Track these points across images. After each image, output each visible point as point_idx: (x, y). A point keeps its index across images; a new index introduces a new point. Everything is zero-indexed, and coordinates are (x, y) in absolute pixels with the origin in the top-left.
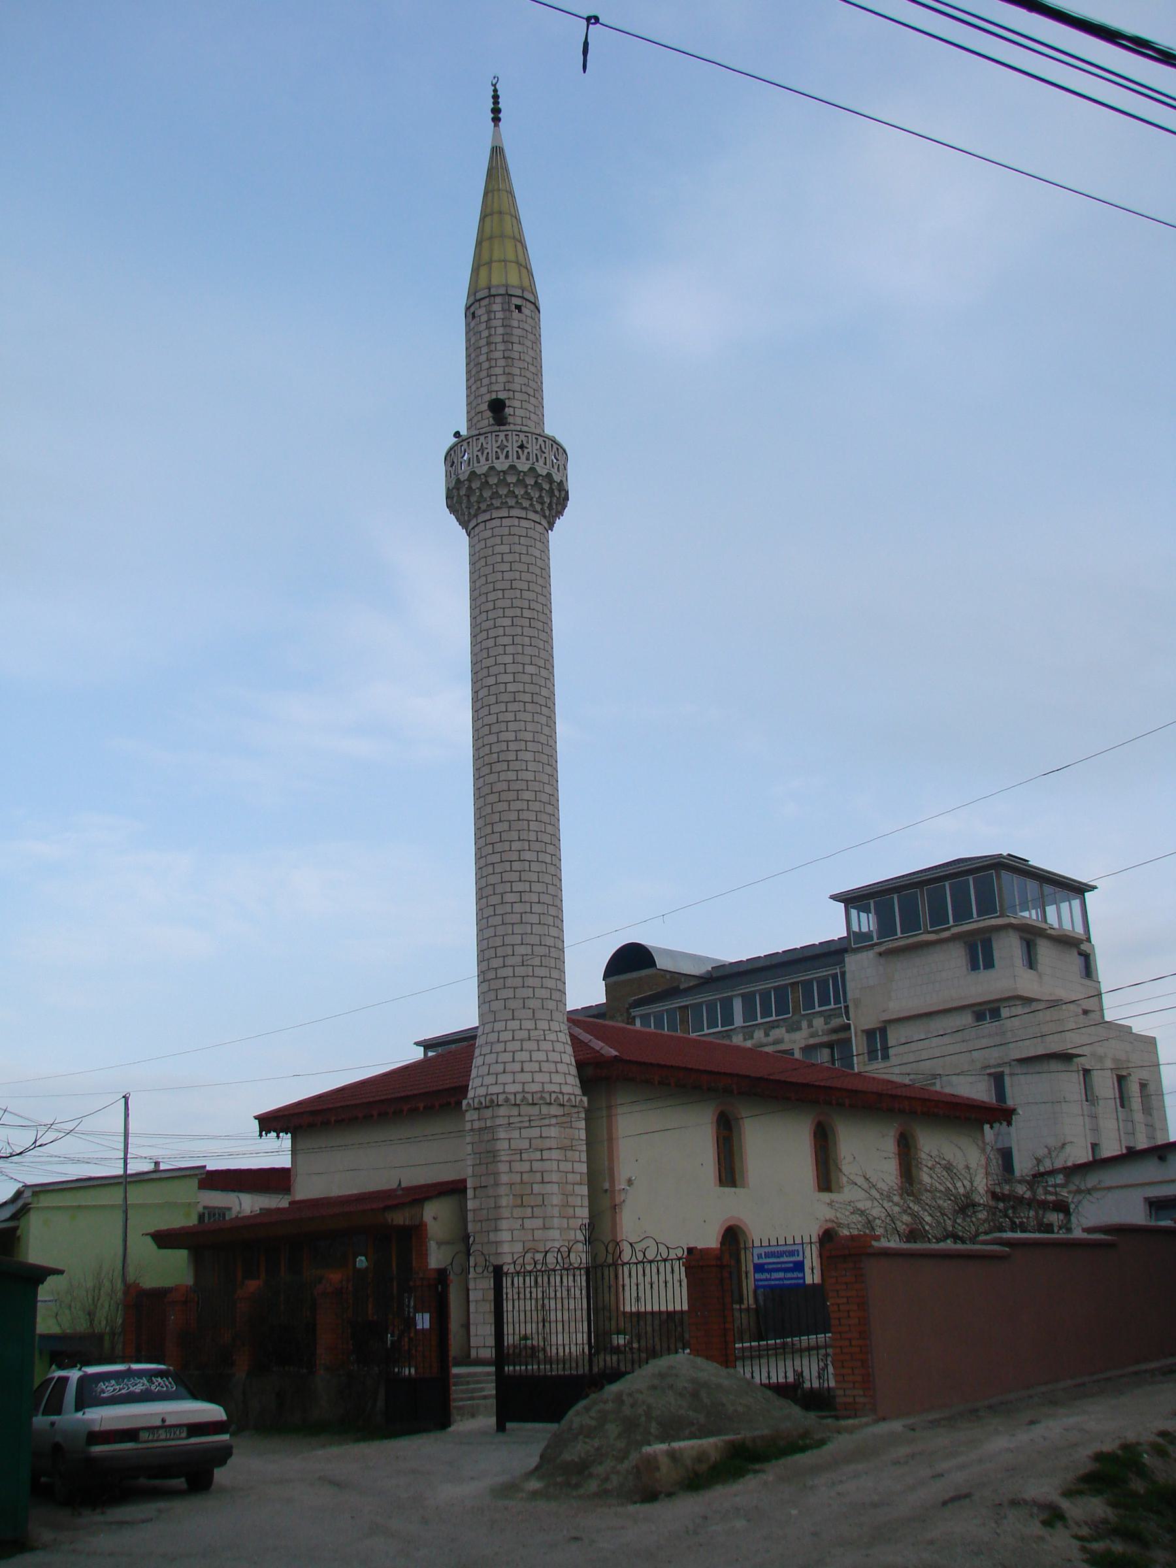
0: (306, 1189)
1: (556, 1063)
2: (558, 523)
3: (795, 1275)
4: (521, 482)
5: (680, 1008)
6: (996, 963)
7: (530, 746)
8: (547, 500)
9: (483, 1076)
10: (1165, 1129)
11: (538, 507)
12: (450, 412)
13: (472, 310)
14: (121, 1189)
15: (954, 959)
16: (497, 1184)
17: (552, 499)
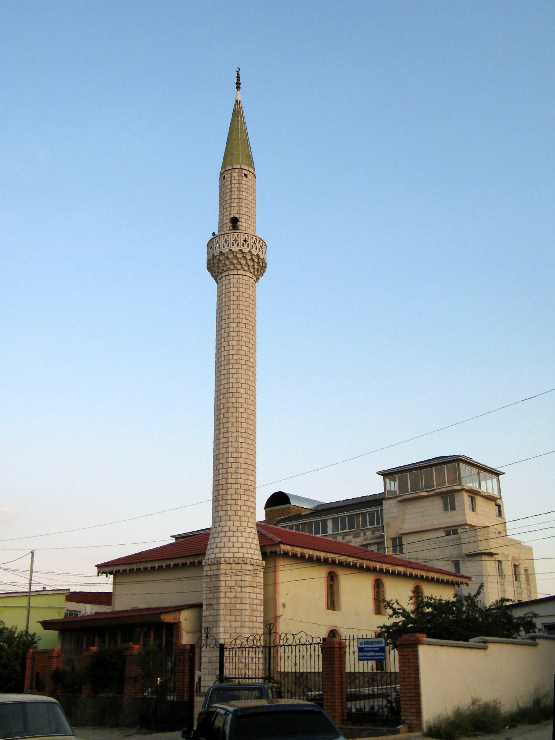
0: (121, 604)
1: (250, 543)
2: (261, 279)
3: (380, 654)
4: (245, 258)
5: (301, 524)
6: (457, 507)
7: (244, 386)
8: (256, 267)
9: (213, 549)
10: (536, 592)
11: (252, 270)
12: (210, 223)
13: (223, 175)
14: (27, 598)
15: (437, 504)
16: (218, 604)
17: (259, 267)
